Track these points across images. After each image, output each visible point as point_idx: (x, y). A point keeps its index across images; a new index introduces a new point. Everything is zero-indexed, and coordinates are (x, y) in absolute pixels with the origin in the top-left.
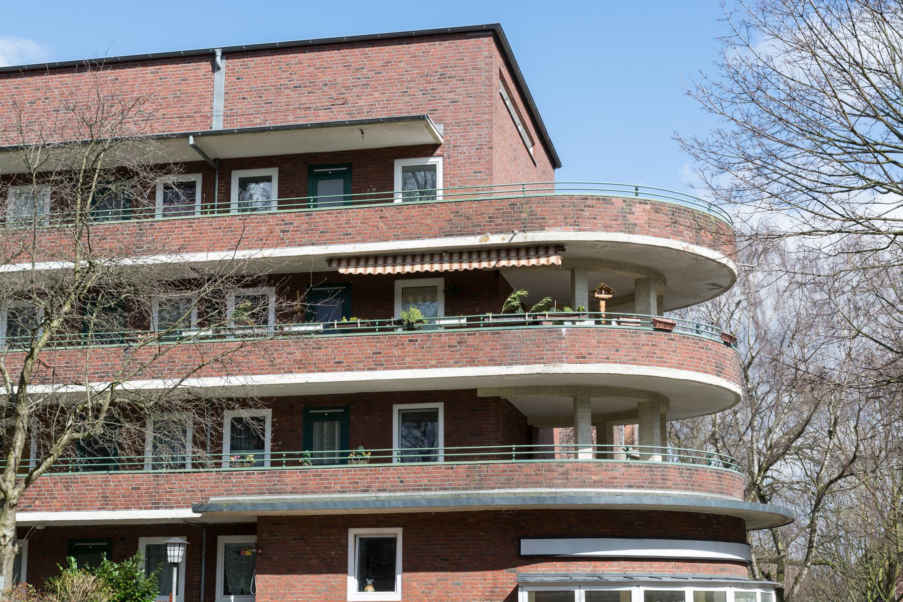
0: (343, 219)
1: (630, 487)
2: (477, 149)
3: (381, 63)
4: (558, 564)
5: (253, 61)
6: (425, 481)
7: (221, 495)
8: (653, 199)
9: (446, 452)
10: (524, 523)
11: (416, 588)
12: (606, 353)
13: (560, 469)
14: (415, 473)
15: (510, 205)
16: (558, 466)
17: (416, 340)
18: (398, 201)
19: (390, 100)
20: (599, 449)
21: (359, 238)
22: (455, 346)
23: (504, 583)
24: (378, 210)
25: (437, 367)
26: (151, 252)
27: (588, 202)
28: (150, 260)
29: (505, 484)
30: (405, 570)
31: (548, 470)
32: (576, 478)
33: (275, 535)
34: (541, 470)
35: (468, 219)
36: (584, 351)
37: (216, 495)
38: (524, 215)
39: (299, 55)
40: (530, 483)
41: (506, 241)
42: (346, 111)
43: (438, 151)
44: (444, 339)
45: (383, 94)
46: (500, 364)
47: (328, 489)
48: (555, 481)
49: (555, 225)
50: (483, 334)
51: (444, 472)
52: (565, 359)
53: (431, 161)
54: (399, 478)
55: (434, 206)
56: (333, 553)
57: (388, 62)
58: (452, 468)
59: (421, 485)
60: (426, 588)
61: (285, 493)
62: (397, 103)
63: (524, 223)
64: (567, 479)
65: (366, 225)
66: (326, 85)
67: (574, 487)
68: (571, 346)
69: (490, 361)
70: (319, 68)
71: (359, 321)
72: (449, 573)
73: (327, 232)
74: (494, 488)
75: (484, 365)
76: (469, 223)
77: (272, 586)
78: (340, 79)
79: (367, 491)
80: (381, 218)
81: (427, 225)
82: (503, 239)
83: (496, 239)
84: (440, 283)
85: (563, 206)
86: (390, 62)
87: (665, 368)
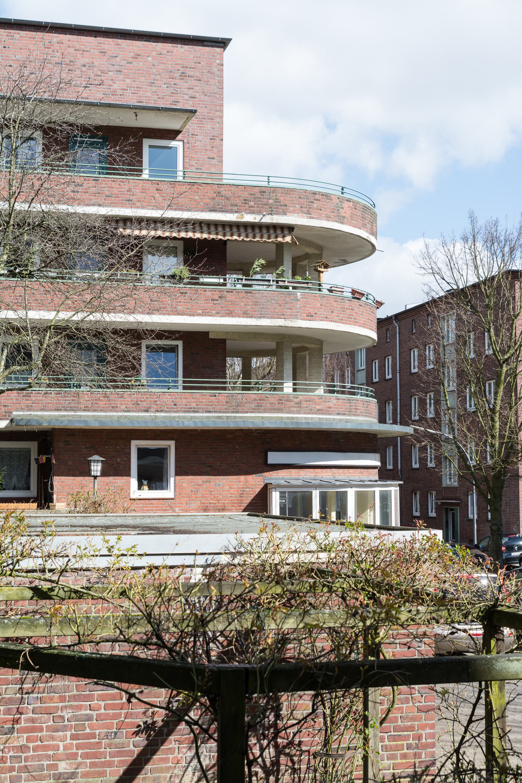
0: (125, 187)
1: (339, 414)
2: (211, 139)
3: (132, 54)
4: (293, 471)
5: (19, 34)
6: (194, 405)
7: (22, 410)
8: (354, 198)
9: (184, 382)
10: (269, 440)
11: (186, 488)
12: (326, 313)
13: (296, 400)
14: (186, 398)
15: (261, 192)
16: (294, 397)
17: (186, 293)
18: (146, 175)
19: (140, 88)
20: (328, 386)
21: (139, 204)
22: (217, 300)
23: (254, 485)
24: (154, 183)
25: (202, 315)
26: (81, 202)
27: (317, 197)
28: (81, 210)
29: (255, 409)
30: (177, 474)
31: (287, 400)
32: (306, 407)
33: (69, 445)
34: (281, 400)
35: (228, 199)
36: (312, 311)
37: (17, 410)
38: (271, 201)
39: (60, 35)
40: (274, 409)
41: (257, 220)
42: (102, 91)
43: (180, 137)
44: (209, 293)
45: (134, 81)
46: (252, 317)
47: (114, 408)
48: (292, 409)
49: (294, 212)
50: (238, 292)
51: (208, 399)
52: (299, 317)
53: (173, 143)
54: (173, 402)
55: (200, 185)
56: (119, 460)
57: (138, 55)
58: (215, 396)
59: (190, 408)
60: (194, 488)
61: (80, 410)
62: (146, 91)
63: (271, 208)
64: (300, 407)
65: (144, 195)
66: (85, 66)
67: (305, 413)
68: (304, 307)
69: (244, 313)
70: (78, 50)
71: (244, 278)
72: (212, 477)
73: (112, 197)
74: (247, 412)
75: (239, 317)
76: (228, 203)
77: (67, 485)
78: (96, 63)
79: (147, 411)
80: (157, 190)
81: (195, 201)
82: (255, 218)
83: (249, 218)
84: (180, 245)
85: (300, 198)
86: (140, 55)
87: (357, 327)
